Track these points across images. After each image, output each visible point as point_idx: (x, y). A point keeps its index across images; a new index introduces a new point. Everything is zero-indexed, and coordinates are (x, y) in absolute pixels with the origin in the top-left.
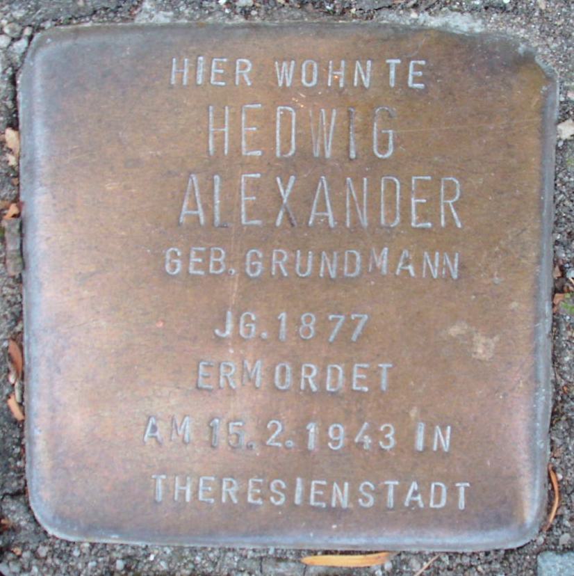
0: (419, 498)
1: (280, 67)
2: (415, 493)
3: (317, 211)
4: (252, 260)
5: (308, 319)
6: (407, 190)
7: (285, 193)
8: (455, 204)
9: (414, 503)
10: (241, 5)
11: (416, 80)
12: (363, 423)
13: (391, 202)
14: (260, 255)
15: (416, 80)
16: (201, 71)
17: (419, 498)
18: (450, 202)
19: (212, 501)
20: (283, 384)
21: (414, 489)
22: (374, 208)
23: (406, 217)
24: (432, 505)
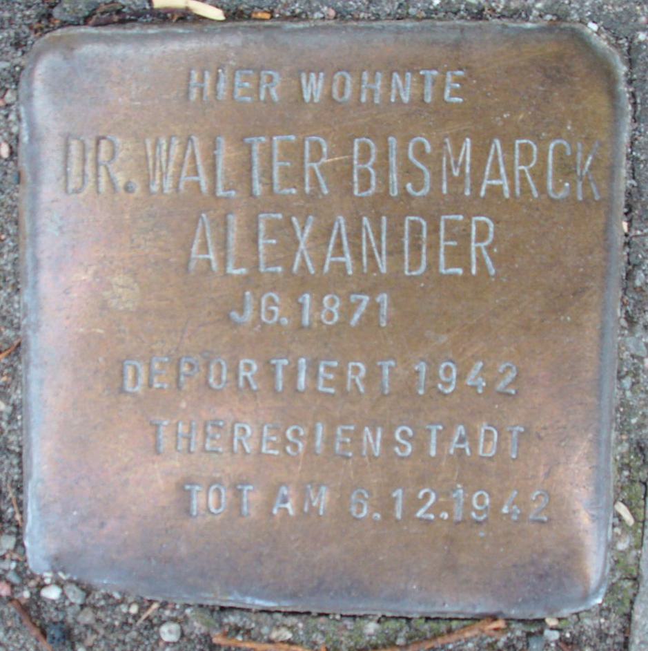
0: (466, 446)
1: (308, 80)
2: (461, 440)
3: (333, 256)
4: (268, 305)
5: (333, 302)
6: (434, 230)
7: (302, 235)
8: (489, 248)
9: (461, 452)
10: (211, 633)
11: (455, 93)
12: (369, 494)
13: (416, 247)
14: (277, 299)
15: (455, 93)
16: (222, 85)
17: (466, 446)
18: (483, 245)
19: (248, 99)
20: (344, 78)
21: (460, 435)
22: (395, 252)
23: (433, 264)
24: (480, 452)
